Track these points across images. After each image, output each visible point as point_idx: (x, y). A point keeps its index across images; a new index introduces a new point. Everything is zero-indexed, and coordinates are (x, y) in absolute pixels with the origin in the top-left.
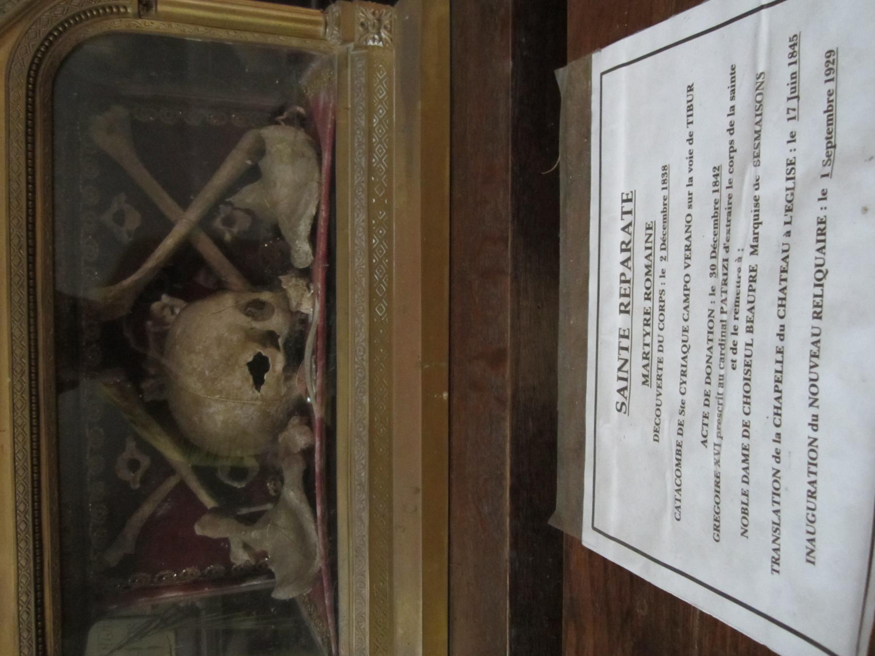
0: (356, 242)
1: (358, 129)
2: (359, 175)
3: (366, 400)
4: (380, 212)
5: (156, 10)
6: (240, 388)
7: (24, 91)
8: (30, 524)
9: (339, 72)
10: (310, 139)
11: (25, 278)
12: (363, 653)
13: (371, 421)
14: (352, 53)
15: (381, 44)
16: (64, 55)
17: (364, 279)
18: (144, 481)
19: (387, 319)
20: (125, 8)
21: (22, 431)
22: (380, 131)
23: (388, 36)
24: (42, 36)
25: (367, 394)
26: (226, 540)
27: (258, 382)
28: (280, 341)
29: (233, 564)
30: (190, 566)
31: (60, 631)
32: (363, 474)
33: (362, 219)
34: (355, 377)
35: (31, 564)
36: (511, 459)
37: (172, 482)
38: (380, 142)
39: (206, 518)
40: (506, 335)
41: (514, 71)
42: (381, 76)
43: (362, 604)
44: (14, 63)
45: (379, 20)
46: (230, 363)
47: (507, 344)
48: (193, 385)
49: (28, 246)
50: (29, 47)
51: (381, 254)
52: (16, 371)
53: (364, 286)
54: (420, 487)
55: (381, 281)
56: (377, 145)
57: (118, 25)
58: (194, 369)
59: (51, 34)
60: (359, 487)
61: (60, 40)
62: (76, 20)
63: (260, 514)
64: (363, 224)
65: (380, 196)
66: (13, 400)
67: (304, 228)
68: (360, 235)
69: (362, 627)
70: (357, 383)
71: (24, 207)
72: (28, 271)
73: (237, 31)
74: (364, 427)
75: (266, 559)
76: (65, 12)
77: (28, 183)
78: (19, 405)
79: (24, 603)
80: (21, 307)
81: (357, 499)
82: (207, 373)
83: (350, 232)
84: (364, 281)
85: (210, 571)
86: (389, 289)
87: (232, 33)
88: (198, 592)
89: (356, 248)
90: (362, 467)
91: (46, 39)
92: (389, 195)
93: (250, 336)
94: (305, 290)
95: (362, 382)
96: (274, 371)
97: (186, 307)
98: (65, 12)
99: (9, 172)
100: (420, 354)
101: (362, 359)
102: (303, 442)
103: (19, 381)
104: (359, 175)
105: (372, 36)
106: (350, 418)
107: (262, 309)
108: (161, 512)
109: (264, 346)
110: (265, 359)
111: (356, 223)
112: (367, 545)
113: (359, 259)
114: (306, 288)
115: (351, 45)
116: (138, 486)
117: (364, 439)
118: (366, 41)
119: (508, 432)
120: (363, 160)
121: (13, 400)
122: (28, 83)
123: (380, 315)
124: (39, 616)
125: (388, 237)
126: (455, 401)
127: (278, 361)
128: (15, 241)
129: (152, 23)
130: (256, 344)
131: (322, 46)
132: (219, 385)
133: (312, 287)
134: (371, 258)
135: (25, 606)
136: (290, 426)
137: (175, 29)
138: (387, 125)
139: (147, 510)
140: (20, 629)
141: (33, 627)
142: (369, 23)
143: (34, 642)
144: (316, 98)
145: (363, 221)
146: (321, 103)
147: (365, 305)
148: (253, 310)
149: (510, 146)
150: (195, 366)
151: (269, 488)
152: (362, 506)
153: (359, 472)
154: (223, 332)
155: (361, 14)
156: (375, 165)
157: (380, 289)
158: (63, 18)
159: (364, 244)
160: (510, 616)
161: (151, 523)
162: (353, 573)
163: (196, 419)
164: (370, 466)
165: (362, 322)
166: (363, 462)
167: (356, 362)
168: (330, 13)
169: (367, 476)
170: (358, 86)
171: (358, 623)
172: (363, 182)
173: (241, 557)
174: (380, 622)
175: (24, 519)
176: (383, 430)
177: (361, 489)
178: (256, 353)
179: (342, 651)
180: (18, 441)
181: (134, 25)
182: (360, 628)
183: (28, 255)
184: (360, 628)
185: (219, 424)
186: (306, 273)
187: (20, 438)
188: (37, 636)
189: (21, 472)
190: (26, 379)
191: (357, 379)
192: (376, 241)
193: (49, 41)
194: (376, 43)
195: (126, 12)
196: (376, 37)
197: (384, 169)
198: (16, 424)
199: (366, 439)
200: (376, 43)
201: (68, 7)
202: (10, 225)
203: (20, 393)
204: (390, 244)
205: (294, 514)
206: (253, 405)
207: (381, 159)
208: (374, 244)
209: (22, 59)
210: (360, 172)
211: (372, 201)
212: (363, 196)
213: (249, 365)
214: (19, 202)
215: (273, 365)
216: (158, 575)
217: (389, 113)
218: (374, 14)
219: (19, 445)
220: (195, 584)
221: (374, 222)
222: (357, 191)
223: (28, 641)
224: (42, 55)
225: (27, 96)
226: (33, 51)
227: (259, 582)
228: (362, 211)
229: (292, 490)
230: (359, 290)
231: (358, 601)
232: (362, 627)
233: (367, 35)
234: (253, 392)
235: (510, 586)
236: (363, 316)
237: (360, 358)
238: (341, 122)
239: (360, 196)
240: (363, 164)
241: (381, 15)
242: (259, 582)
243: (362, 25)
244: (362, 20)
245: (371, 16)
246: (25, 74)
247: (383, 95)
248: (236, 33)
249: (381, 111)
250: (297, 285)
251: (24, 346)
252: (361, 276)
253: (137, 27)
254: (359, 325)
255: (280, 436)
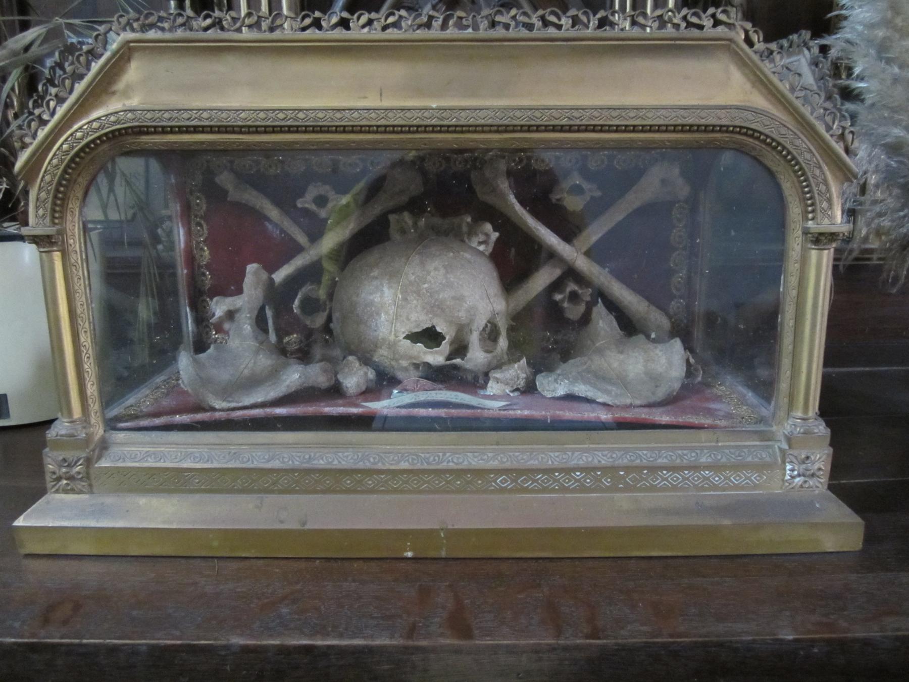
0: (577, 454)
1: (697, 454)
2: (649, 456)
3: (404, 465)
4: (609, 480)
5: (813, 249)
6: (408, 319)
7: (727, 123)
8: (283, 123)
9: (756, 432)
10: (675, 393)
11: (539, 122)
12: (119, 460)
13: (379, 472)
14: (776, 446)
15: (788, 477)
16: (761, 159)
17: (536, 462)
18: (306, 212)
19: (493, 488)
20: (813, 219)
21: (381, 117)
22: (696, 479)
23: (797, 484)
24: (781, 140)
25: (411, 467)
26: (239, 291)
27: (414, 337)
28: (457, 361)
29: (211, 299)
30: (210, 253)
31: (166, 148)
32: (321, 462)
33: (601, 460)
34: (428, 453)
35: (240, 123)
36: (346, 646)
37: (302, 239)
38: (684, 479)
39: (264, 275)
40: (488, 638)
41: (782, 641)
42: (754, 478)
43: (176, 458)
44: (755, 114)
45: (813, 475)
46: (435, 309)
47: (478, 640)
48: (412, 270)
49: (571, 126)
50: (771, 128)
51: (564, 481)
52: (443, 113)
53: (529, 463)
54: (307, 527)
55: (534, 481)
56: (680, 475)
57: (794, 210)
58: (429, 273)
59: (784, 148)
60: (307, 457)
61: (778, 157)
62: (798, 172)
63: (266, 331)
64: (596, 461)
65: (627, 479)
66: (414, 110)
67: (581, 389)
68: (584, 458)
69: (149, 459)
70: (423, 455)
71: (611, 123)
72: (546, 126)
73: (794, 328)
74: (375, 463)
75: (214, 333)
76: (807, 162)
77: (634, 126)
78: (408, 114)
79: (200, 115)
80: (509, 119)
81: (294, 454)
82: (426, 286)
83: (586, 446)
84: (534, 463)
85: (204, 274)
86: (526, 490)
87: (792, 323)
88: (183, 264)
89: (570, 454)
90: (330, 460)
91: (779, 144)
92: (628, 488)
93: (462, 331)
94: (512, 387)
95: (423, 461)
96: (425, 353)
97: (485, 255)
98: (807, 162)
99: (646, 109)
100: (456, 527)
101: (449, 462)
102: (349, 385)
103: (433, 115)
104: (649, 455)
105: (796, 468)
106: (384, 447)
107: (489, 338)
108: (270, 227)
109: (452, 343)
110: (439, 345)
111: (596, 452)
112: (244, 466)
113: (558, 457)
114: (515, 388)
115: (785, 446)
116: (299, 205)
117: (361, 463)
118: (791, 462)
119: (378, 642)
120: (665, 461)
121: (414, 110)
122: (735, 127)
123: (498, 481)
124: (185, 129)
125: (583, 489)
126: (402, 565)
127: (436, 357)
128: (576, 114)
129: (798, 244)
130: (454, 334)
131: (782, 414)
132: (412, 298)
133: (516, 394)
134: (560, 470)
135: (196, 116)
136: (365, 369)
137: (792, 266)
138: (703, 486)
139: (273, 213)
140: (173, 110)
141: (174, 123)
142: (809, 465)
143: (157, 124)
144: (718, 398)
145: (600, 462)
146: (713, 406)
147: (508, 465)
148: (488, 329)
149: (700, 639)
150: (432, 274)
151: (291, 337)
152: (286, 460)
153: (324, 457)
154: (468, 302)
155: (818, 456)
156: (660, 473)
157: (526, 481)
158: (800, 160)
159: (575, 462)
160: (163, 644)
161: (260, 217)
162: (210, 449)
163: (375, 273)
164: (331, 470)
165: (490, 461)
166: (336, 462)
167: (444, 454)
168: (817, 423)
169: (321, 467)
170: (743, 454)
171: (154, 453)
172: (641, 460)
173: (219, 307)
174: (154, 478)
175: (289, 117)
176: (370, 485)
177: (305, 459)
178: (445, 336)
179: (123, 435)
180: (371, 114)
181: (796, 227)
182: (148, 455)
183: (562, 126)
184: (148, 455)
185: (371, 297)
186: (530, 389)
187: (373, 115)
188: (163, 127)
189: (338, 115)
190: (434, 122)
191: (428, 455)
192: (578, 476)
193: (775, 145)
194: (788, 472)
195: (808, 219)
196: (796, 473)
197: (656, 483)
198: (388, 111)
199: (361, 465)
200: (788, 472)
201: (811, 165)
202: (593, 109)
203: (420, 116)
204: (574, 491)
205: (273, 375)
206: (391, 332)
207: (666, 479)
208: (575, 474)
209: (758, 122)
210: (651, 457)
211: (622, 471)
212: (625, 461)
213: (434, 327)
214: (616, 117)
215: (431, 352)
216: (202, 222)
217: (715, 487)
218: (820, 469)
219: (367, 114)
220: (191, 259)
221: (599, 473)
222: (630, 454)
223: (159, 118)
224: (763, 139)
225: (721, 126)
226: (767, 132)
227: (190, 329)
228: (611, 460)
229: (300, 377)
230: (525, 457)
231: (179, 454)
232: (149, 459)
233: (797, 462)
234: (404, 333)
235: (197, 644)
236: (496, 462)
237: (450, 458)
238: (703, 435)
239: (626, 457)
240: (659, 461)
241: (818, 477)
242: (190, 329)
243: (808, 458)
244: (813, 458)
245: (816, 466)
246: (742, 124)
247: (734, 480)
248: (792, 326)
249: (717, 479)
250: (518, 378)
251: (469, 120)
252: (540, 459)
253: (793, 229)
254: (486, 457)
255: (354, 357)
